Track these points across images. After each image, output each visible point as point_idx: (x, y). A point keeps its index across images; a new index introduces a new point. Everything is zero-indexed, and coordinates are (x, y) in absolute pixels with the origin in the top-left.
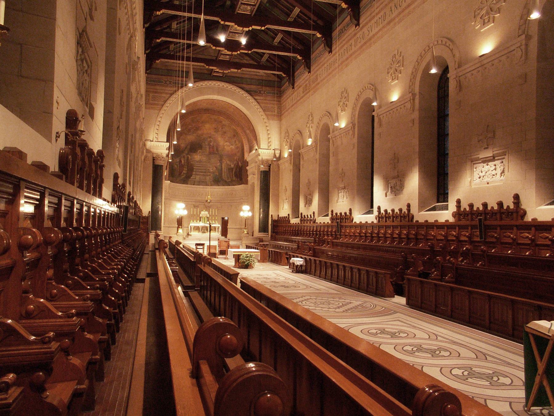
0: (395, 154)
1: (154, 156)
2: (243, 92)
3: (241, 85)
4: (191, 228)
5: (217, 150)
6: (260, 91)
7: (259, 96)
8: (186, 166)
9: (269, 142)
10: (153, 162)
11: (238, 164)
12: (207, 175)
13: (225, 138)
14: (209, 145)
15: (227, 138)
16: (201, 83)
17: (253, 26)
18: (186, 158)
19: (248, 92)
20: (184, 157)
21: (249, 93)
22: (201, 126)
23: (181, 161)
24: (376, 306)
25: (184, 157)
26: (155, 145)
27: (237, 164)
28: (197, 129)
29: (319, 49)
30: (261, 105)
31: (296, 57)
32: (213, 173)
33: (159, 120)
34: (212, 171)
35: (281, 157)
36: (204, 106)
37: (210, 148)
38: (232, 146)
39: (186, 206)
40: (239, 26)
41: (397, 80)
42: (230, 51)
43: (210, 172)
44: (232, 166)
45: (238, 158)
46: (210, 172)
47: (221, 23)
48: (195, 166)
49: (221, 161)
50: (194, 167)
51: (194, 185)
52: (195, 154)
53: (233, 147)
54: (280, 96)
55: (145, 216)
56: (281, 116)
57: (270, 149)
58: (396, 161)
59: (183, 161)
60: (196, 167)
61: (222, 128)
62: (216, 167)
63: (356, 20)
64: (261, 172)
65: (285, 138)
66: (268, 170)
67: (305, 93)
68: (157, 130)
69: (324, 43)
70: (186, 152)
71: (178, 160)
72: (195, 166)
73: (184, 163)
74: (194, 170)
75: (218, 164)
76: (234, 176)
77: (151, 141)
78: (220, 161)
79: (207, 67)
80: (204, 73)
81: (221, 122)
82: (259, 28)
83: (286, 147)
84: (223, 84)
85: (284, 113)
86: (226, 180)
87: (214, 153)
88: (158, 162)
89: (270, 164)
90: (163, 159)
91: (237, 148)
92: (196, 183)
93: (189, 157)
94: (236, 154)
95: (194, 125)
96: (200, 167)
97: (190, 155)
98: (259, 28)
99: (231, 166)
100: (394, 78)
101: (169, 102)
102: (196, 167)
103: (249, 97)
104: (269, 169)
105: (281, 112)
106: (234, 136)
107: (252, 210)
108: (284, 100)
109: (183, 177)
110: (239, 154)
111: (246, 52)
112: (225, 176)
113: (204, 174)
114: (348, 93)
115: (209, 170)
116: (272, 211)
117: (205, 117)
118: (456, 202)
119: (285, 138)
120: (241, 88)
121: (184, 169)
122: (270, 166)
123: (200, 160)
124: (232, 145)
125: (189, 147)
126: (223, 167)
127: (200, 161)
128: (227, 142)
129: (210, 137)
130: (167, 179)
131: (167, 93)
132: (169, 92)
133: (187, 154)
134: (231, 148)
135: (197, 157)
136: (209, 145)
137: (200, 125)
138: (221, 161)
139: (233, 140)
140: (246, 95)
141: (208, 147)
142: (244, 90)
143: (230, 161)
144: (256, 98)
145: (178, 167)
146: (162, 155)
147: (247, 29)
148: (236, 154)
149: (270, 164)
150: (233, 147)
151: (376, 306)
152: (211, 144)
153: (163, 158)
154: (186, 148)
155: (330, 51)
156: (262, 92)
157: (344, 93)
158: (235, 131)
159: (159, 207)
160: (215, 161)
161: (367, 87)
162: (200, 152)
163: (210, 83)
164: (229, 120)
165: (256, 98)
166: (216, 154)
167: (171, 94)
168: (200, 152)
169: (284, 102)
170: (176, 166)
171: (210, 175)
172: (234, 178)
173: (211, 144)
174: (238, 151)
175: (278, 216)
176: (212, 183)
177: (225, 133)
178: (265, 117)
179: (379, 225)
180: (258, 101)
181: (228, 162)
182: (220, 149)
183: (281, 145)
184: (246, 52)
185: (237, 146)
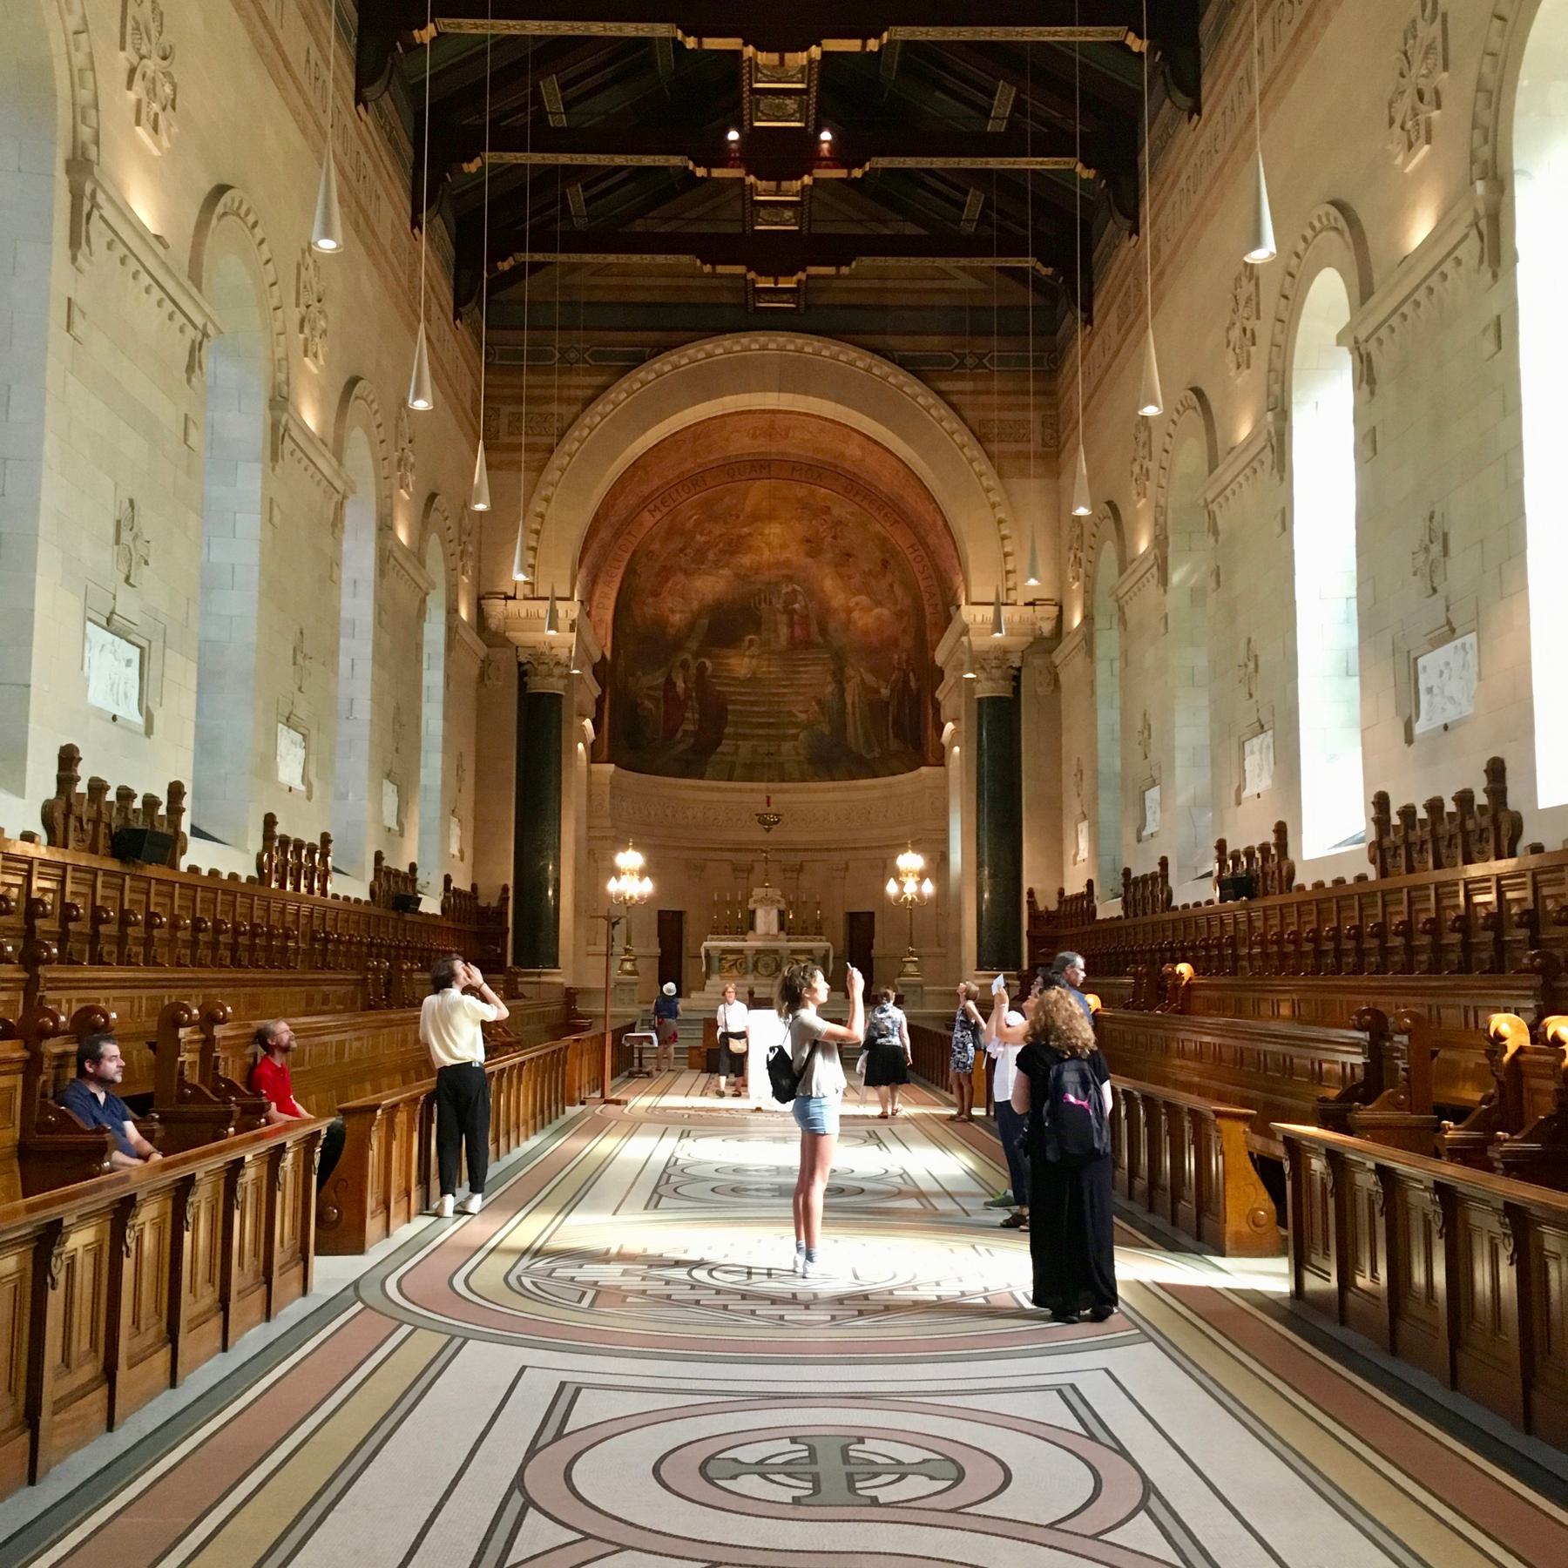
0: (1431, 518)
1: (523, 659)
2: (882, 368)
3: (877, 340)
4: (708, 956)
5: (823, 631)
6: (962, 357)
7: (962, 377)
8: (695, 704)
9: (1008, 572)
10: (522, 686)
11: (906, 682)
12: (785, 738)
13: (850, 577)
14: (789, 612)
15: (857, 579)
16: (708, 347)
17: (824, 42)
18: (693, 671)
19: (908, 364)
20: (685, 665)
21: (909, 371)
22: (750, 534)
23: (670, 683)
24: (506, 1279)
25: (685, 665)
26: (523, 614)
27: (900, 685)
28: (736, 546)
29: (1156, 112)
30: (968, 414)
31: (1073, 171)
32: (808, 726)
33: (538, 510)
34: (803, 716)
35: (1065, 629)
36: (743, 444)
37: (791, 625)
38: (877, 611)
39: (649, 861)
40: (760, 48)
41: (1428, 141)
42: (767, 180)
43: (795, 725)
44: (885, 692)
45: (904, 656)
46: (795, 725)
47: (688, 46)
48: (734, 702)
49: (840, 680)
50: (730, 707)
51: (730, 779)
52: (730, 652)
53: (885, 612)
54: (1051, 370)
55: (488, 907)
56: (1058, 455)
57: (1014, 604)
58: (1436, 549)
59: (680, 685)
60: (738, 707)
61: (834, 537)
62: (819, 702)
63: (1187, 94)
64: (980, 700)
65: (1070, 549)
66: (1009, 695)
67: (1123, 332)
68: (531, 553)
69: (1163, 73)
70: (693, 645)
71: (661, 681)
72: (734, 702)
73: (686, 688)
74: (730, 717)
75: (829, 689)
76: (891, 735)
77: (507, 598)
78: (834, 674)
79: (707, 268)
80: (722, 305)
81: (827, 510)
82: (853, 45)
83: (1076, 586)
84: (800, 341)
85: (1066, 441)
86: (863, 752)
87: (807, 644)
88: (538, 685)
89: (1019, 669)
90: (557, 671)
91: (899, 615)
92: (738, 771)
93: (708, 663)
94: (896, 643)
95: (718, 529)
96: (753, 703)
97: (709, 656)
98: (853, 45)
99: (877, 691)
100: (1413, 138)
101: (575, 433)
102: (738, 707)
103: (913, 387)
104: (1017, 690)
105: (1058, 437)
106: (885, 564)
107: (938, 867)
108: (1066, 383)
109: (682, 747)
110: (907, 642)
111: (841, 173)
112: (855, 735)
113: (772, 732)
114: (1445, 16)
115: (790, 713)
116: (1032, 877)
117: (757, 493)
118: (1485, 771)
119: (1070, 549)
120: (875, 351)
121: (688, 715)
122: (1017, 679)
123: (754, 673)
124: (879, 604)
125: (705, 622)
126: (849, 699)
127: (753, 680)
128: (859, 592)
129: (790, 579)
130: (605, 755)
131: (569, 401)
132: (580, 393)
133: (696, 655)
134: (879, 618)
135: (741, 664)
136: (789, 612)
137: (746, 530)
138: (840, 680)
139: (885, 583)
140: (898, 377)
141: (783, 619)
142: (893, 361)
143: (875, 671)
144: (944, 386)
145: (658, 708)
146: (554, 652)
147: (801, 58)
148: (896, 643)
149: (1019, 669)
150: (885, 612)
151: (451, 1279)
152: (797, 606)
153: (558, 663)
154: (691, 627)
155: (1196, 109)
156: (969, 361)
157: (1244, 281)
158: (883, 542)
159: (545, 868)
160: (815, 676)
161: (1317, 224)
162: (751, 641)
163: (745, 341)
164: (857, 499)
165: (944, 386)
166: (818, 646)
167: (589, 402)
168: (751, 642)
169: (1066, 392)
170: (648, 704)
171: (795, 737)
172: (894, 745)
173: (797, 606)
174: (904, 631)
175: (1061, 892)
176: (806, 766)
177: (849, 555)
178: (982, 465)
179: (1360, 891)
180: (954, 399)
181: (870, 679)
182: (832, 626)
183: (1061, 584)
184: (841, 173)
185: (899, 607)
